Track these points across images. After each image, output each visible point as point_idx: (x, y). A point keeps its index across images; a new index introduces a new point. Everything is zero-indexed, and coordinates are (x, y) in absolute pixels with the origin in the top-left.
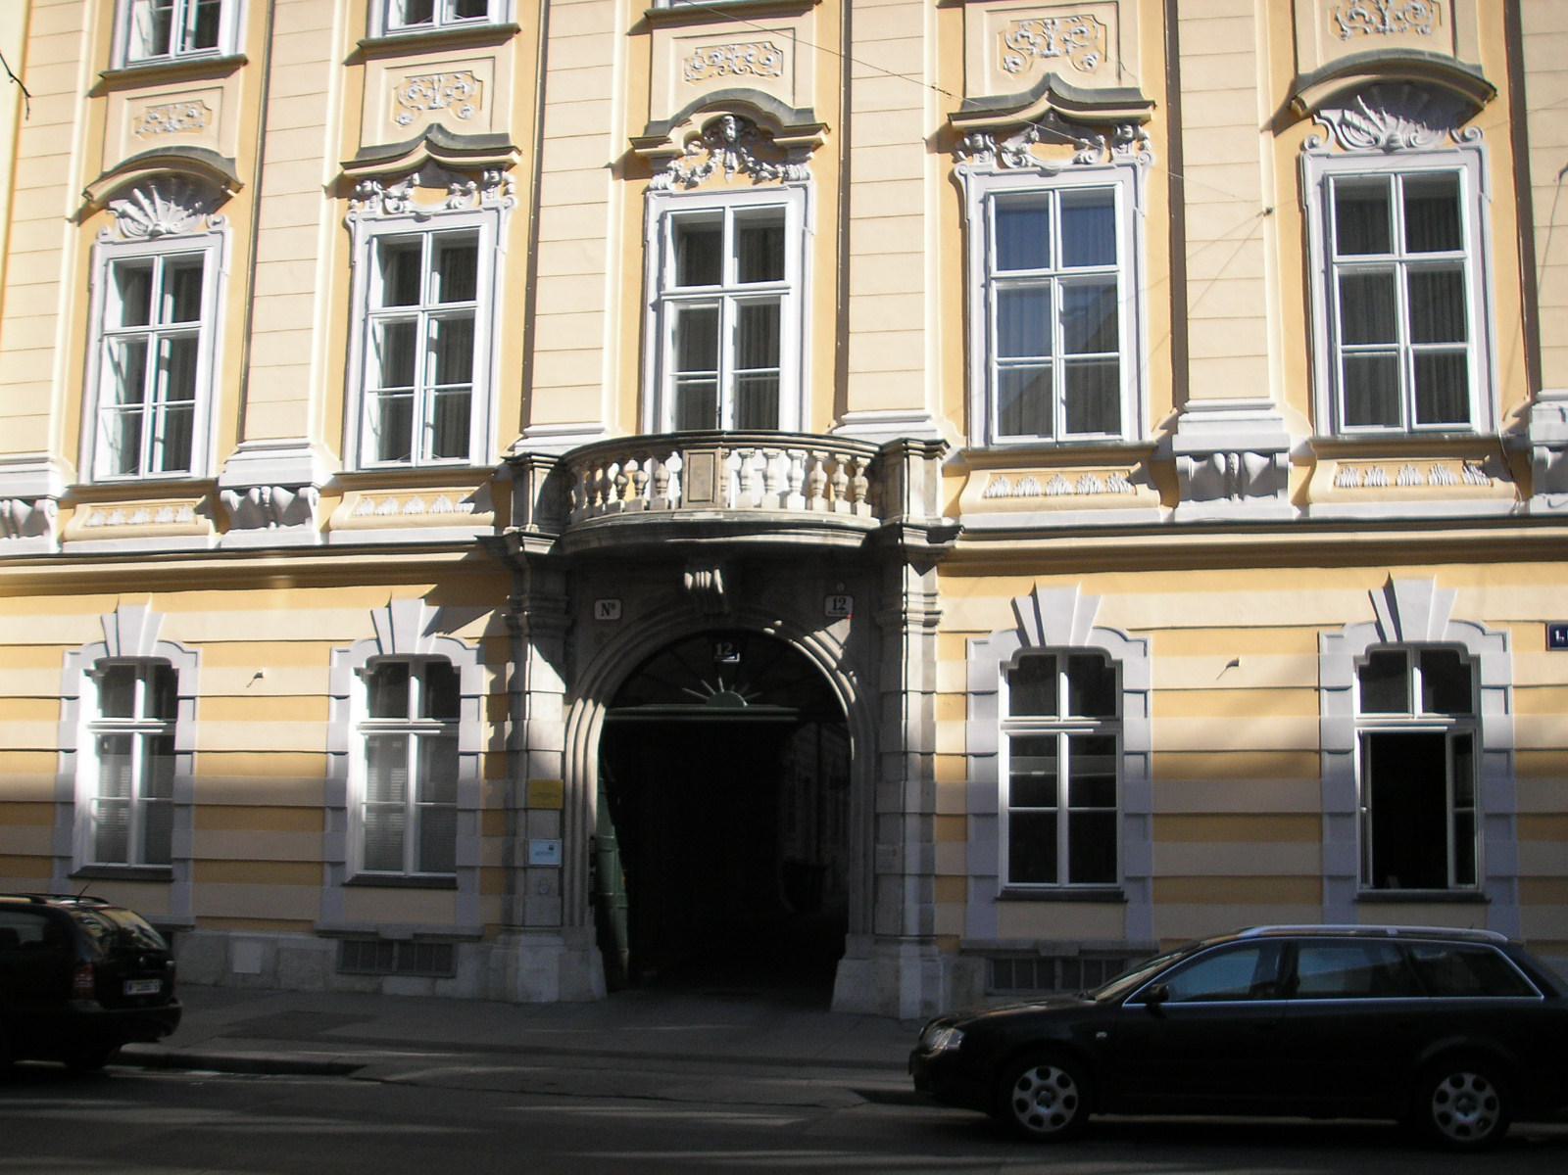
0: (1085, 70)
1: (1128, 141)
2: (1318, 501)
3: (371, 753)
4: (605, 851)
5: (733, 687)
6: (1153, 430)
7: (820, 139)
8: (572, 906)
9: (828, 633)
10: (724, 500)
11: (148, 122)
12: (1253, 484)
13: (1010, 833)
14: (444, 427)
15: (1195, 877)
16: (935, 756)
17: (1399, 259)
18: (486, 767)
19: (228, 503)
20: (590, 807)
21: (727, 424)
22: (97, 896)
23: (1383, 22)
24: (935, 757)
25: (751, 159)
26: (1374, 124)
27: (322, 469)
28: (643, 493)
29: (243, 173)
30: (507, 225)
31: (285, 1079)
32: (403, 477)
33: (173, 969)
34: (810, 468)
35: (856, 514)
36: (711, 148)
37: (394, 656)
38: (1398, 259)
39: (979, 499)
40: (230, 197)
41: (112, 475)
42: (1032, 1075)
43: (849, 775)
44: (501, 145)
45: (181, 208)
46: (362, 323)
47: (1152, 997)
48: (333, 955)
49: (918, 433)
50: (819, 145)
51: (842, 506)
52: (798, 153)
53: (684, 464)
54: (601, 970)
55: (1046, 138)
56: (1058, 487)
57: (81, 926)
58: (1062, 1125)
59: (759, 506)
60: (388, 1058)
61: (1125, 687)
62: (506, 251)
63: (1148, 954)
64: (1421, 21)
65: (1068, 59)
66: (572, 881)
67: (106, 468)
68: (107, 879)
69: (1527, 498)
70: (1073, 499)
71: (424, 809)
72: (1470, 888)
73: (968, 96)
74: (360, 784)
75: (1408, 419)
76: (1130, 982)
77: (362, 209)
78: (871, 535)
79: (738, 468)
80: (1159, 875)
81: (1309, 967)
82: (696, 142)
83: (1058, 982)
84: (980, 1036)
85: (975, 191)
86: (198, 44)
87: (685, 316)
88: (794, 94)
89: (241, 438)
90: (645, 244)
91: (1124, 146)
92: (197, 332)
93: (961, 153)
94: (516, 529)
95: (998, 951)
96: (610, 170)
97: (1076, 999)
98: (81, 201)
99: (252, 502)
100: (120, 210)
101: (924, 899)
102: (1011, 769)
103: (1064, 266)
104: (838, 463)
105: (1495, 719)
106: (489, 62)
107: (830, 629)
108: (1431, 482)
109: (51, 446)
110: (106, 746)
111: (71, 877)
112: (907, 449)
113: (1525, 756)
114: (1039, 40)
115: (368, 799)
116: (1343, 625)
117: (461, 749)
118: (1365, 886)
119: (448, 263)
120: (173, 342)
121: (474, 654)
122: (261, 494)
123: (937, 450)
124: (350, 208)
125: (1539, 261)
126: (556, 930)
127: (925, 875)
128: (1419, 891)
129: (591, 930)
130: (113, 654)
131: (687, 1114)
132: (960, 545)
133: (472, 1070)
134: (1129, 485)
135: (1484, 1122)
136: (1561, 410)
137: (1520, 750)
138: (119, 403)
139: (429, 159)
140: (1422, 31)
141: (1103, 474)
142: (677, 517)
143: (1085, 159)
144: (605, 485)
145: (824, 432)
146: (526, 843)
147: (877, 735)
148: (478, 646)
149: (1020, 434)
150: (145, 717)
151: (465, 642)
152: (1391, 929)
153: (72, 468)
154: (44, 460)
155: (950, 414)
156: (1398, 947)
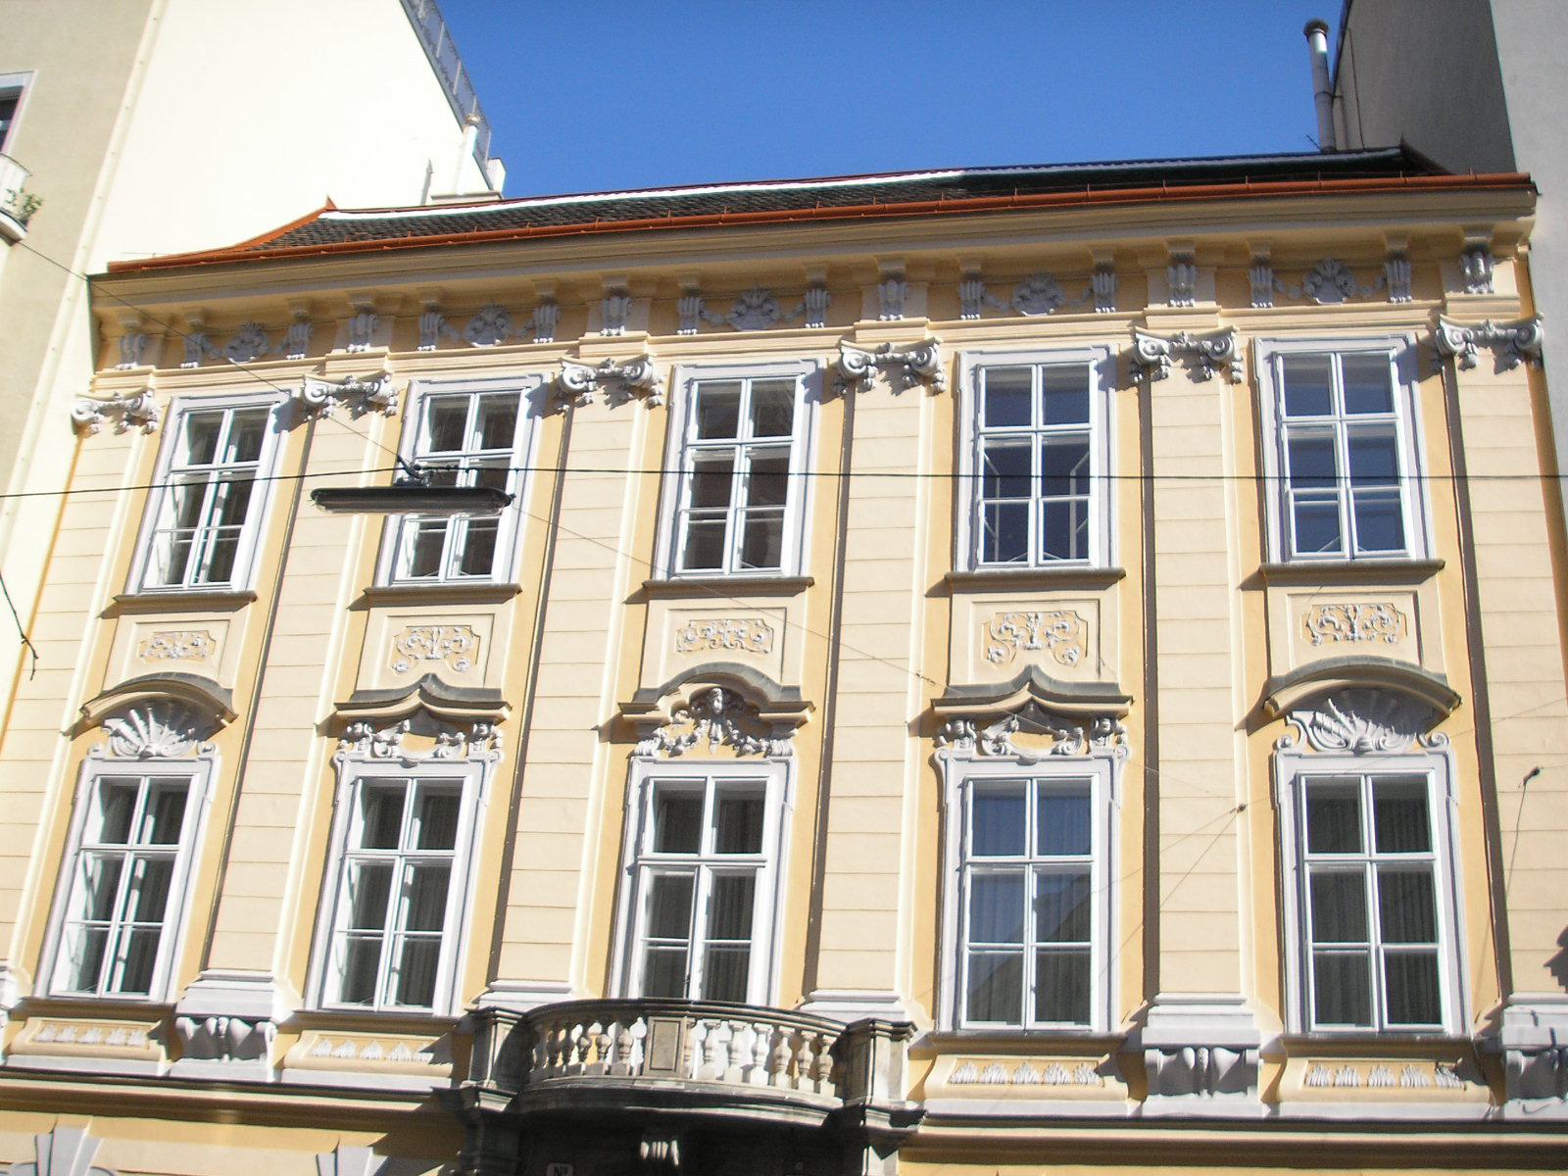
0: (1066, 664)
1: (1106, 735)
2: (1288, 1100)
7: (805, 717)
10: (686, 1070)
17: (1370, 859)
19: (183, 1030)
21: (695, 993)
23: (1352, 630)
25: (737, 732)
27: (282, 1005)
28: (605, 1057)
29: (239, 705)
30: (491, 779)
32: (365, 1021)
34: (775, 1043)
38: (1368, 858)
40: (222, 727)
41: (69, 990)
44: (491, 700)
45: (174, 732)
46: (339, 863)
49: (886, 1014)
50: (803, 722)
51: (806, 1084)
52: (782, 729)
53: (648, 1031)
55: (1025, 728)
59: (721, 1078)
64: (1387, 629)
67: (64, 983)
69: (1502, 1102)
70: (1039, 1088)
73: (951, 683)
75: (1380, 1019)
77: (350, 750)
78: (833, 1116)
79: (703, 1039)
82: (683, 712)
85: (954, 776)
86: (211, 578)
87: (660, 883)
88: (782, 671)
89: (204, 966)
90: (626, 808)
91: (1101, 739)
93: (942, 738)
94: (474, 1083)
96: (597, 732)
98: (78, 717)
99: (208, 1032)
103: (1039, 854)
106: (489, 619)
109: (12, 955)
112: (874, 1030)
114: (1022, 633)
119: (430, 807)
120: (149, 864)
122: (218, 1025)
124: (339, 748)
125: (1506, 866)
132: (922, 1130)
134: (1097, 1076)
136: (1533, 1014)
138: (86, 918)
139: (421, 707)
140: (1389, 640)
141: (1070, 1064)
143: (1063, 750)
144: (567, 1047)
145: (791, 1008)
153: (30, 981)
155: (919, 997)
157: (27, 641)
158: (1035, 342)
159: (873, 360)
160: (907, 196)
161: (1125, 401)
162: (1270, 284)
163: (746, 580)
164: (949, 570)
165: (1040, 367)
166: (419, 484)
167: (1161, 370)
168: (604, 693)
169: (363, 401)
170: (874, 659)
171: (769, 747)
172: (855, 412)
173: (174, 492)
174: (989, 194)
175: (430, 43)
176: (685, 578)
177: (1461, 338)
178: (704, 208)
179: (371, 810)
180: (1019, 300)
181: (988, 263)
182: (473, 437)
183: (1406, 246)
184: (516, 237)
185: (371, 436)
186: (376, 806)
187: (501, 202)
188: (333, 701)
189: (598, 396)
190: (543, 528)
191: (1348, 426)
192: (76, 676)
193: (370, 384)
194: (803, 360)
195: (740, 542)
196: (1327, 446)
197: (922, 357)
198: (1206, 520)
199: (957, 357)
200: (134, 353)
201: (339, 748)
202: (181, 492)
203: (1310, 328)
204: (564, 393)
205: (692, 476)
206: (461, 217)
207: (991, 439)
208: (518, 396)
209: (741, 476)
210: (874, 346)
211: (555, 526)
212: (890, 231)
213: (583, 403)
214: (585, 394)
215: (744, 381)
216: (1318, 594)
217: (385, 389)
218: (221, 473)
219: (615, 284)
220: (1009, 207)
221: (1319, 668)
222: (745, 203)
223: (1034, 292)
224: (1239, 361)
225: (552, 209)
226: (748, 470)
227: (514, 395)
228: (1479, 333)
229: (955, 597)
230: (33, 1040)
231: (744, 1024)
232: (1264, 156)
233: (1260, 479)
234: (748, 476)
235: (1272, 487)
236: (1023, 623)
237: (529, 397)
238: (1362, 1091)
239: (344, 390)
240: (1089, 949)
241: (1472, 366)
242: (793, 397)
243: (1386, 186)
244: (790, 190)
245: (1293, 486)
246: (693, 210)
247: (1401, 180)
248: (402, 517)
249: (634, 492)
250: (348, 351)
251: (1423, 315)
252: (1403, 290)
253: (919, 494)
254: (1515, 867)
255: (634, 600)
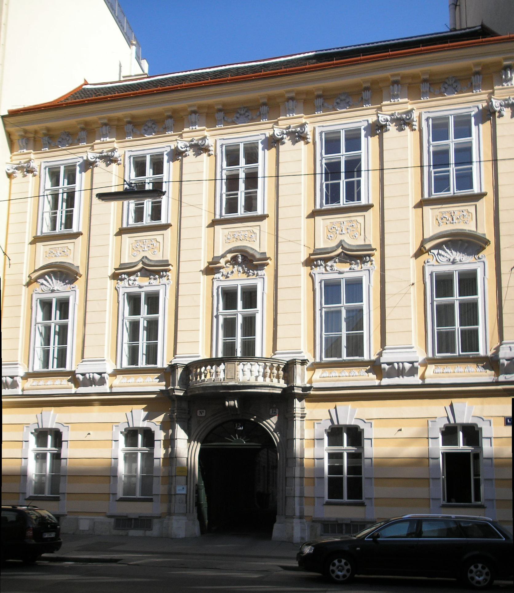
0: (354, 239)
1: (367, 262)
3: (125, 458)
4: (200, 489)
5: (241, 437)
6: (374, 356)
8: (190, 507)
9: (271, 420)
10: (238, 378)
11: (49, 253)
12: (407, 373)
13: (328, 483)
14: (149, 355)
15: (388, 498)
16: (304, 459)
17: (456, 299)
18: (163, 463)
19: (79, 378)
20: (196, 475)
21: (239, 354)
22: (34, 506)
23: (453, 220)
24: (304, 459)
25: (246, 269)
26: (449, 254)
27: (109, 368)
29: (82, 271)
31: (96, 564)
33: (59, 529)
34: (265, 368)
35: (279, 383)
36: (233, 265)
37: (133, 427)
38: (456, 298)
39: (318, 378)
42: (336, 561)
43: (277, 465)
44: (166, 263)
45: (61, 282)
47: (374, 537)
48: (113, 524)
50: (268, 264)
51: (275, 380)
52: (261, 267)
53: (225, 367)
54: (199, 527)
55: (340, 262)
56: (343, 374)
57: (29, 515)
58: (346, 578)
59: (249, 380)
60: (130, 557)
61: (365, 437)
62: (168, 298)
63: (373, 523)
64: (465, 219)
65: (348, 235)
66: (190, 499)
67: (38, 367)
68: (38, 500)
69: (498, 376)
70: (348, 378)
71: (142, 476)
72: (479, 503)
73: (315, 248)
74: (122, 468)
75: (458, 351)
76: (367, 532)
77: (121, 284)
78: (284, 390)
79: (242, 368)
80: (376, 497)
81: (426, 528)
83: (344, 531)
84: (319, 548)
85: (317, 279)
86: (66, 228)
87: (225, 320)
88: (260, 247)
89: (83, 358)
90: (213, 296)
91: (366, 263)
92: (68, 323)
93: (313, 267)
94: (172, 387)
95: (325, 521)
96: (201, 272)
97: (350, 537)
98: (28, 279)
99: (87, 378)
100: (41, 283)
101: (301, 504)
102: (328, 463)
103: (346, 303)
104: (274, 367)
105: (487, 448)
106: (162, 236)
107: (271, 419)
108: (466, 371)
109: (19, 359)
110: (38, 457)
111: (26, 499)
112: (295, 362)
113: (497, 460)
114: (339, 229)
115: (125, 473)
116: (436, 418)
117: (155, 457)
118: (444, 502)
120: (60, 326)
121: (159, 427)
122: (90, 376)
123: (305, 363)
124: (117, 283)
125: (503, 298)
126: (185, 514)
127: (301, 497)
128: (462, 504)
129: (196, 515)
130: (41, 427)
131: (226, 574)
132: (312, 392)
133: (157, 560)
135: (485, 580)
136: (510, 347)
137: (496, 458)
138: (42, 346)
139: (143, 268)
140: (466, 223)
141: (358, 370)
142: (223, 384)
144: (200, 374)
145: (269, 357)
146: (175, 487)
147: (286, 452)
148: (160, 424)
149: (331, 357)
150: (51, 447)
151: (156, 423)
152: (453, 516)
154: (17, 364)
155: (309, 351)
156: (455, 522)
157: (5, 254)
158: (341, 121)
159: (285, 132)
160: (294, 64)
161: (374, 141)
162: (428, 89)
163: (246, 216)
164: (314, 208)
165: (344, 130)
166: (133, 189)
167: (387, 128)
168: (202, 259)
169: (109, 160)
170: (290, 241)
171: (257, 273)
172: (280, 153)
173: (47, 197)
174: (324, 61)
175: (113, 9)
176: (226, 217)
177: (499, 105)
178: (222, 76)
179: (130, 303)
180: (336, 104)
181: (325, 90)
182: (149, 171)
183: (480, 69)
184: (155, 92)
185: (114, 173)
186: (132, 302)
187: (148, 77)
188: (113, 268)
189: (191, 153)
190: (177, 203)
191: (454, 144)
192: (25, 265)
193: (110, 153)
194: (261, 134)
195: (243, 203)
196: (446, 152)
197: (302, 130)
198: (402, 183)
199: (314, 129)
200: (24, 146)
201: (117, 283)
202: (50, 197)
203: (442, 106)
204: (179, 152)
205: (225, 180)
206: (134, 84)
207: (327, 159)
208: (163, 154)
209: (242, 179)
210: (285, 127)
211: (181, 202)
212: (289, 80)
213: (186, 156)
214: (186, 152)
215: (241, 144)
216: (441, 208)
217: (116, 155)
218: (63, 189)
219: (193, 109)
220: (332, 66)
221: (441, 234)
222: (236, 72)
223: (341, 100)
224: (416, 122)
225: (167, 79)
226: (244, 177)
227: (161, 154)
228: (506, 102)
229: (316, 217)
230: (31, 385)
231: (255, 363)
232: (428, 35)
233: (422, 167)
234: (244, 179)
235: (426, 169)
236: (339, 225)
237: (167, 154)
238: (452, 374)
239: (102, 155)
240: (363, 333)
241: (502, 116)
242: (258, 148)
243: (474, 43)
244: (252, 65)
245: (433, 169)
246: (218, 76)
247: (481, 40)
248: (128, 202)
249: (206, 188)
250: (101, 141)
251: (485, 97)
252: (478, 87)
253: (303, 182)
254: (506, 299)
255: (309, 217)
